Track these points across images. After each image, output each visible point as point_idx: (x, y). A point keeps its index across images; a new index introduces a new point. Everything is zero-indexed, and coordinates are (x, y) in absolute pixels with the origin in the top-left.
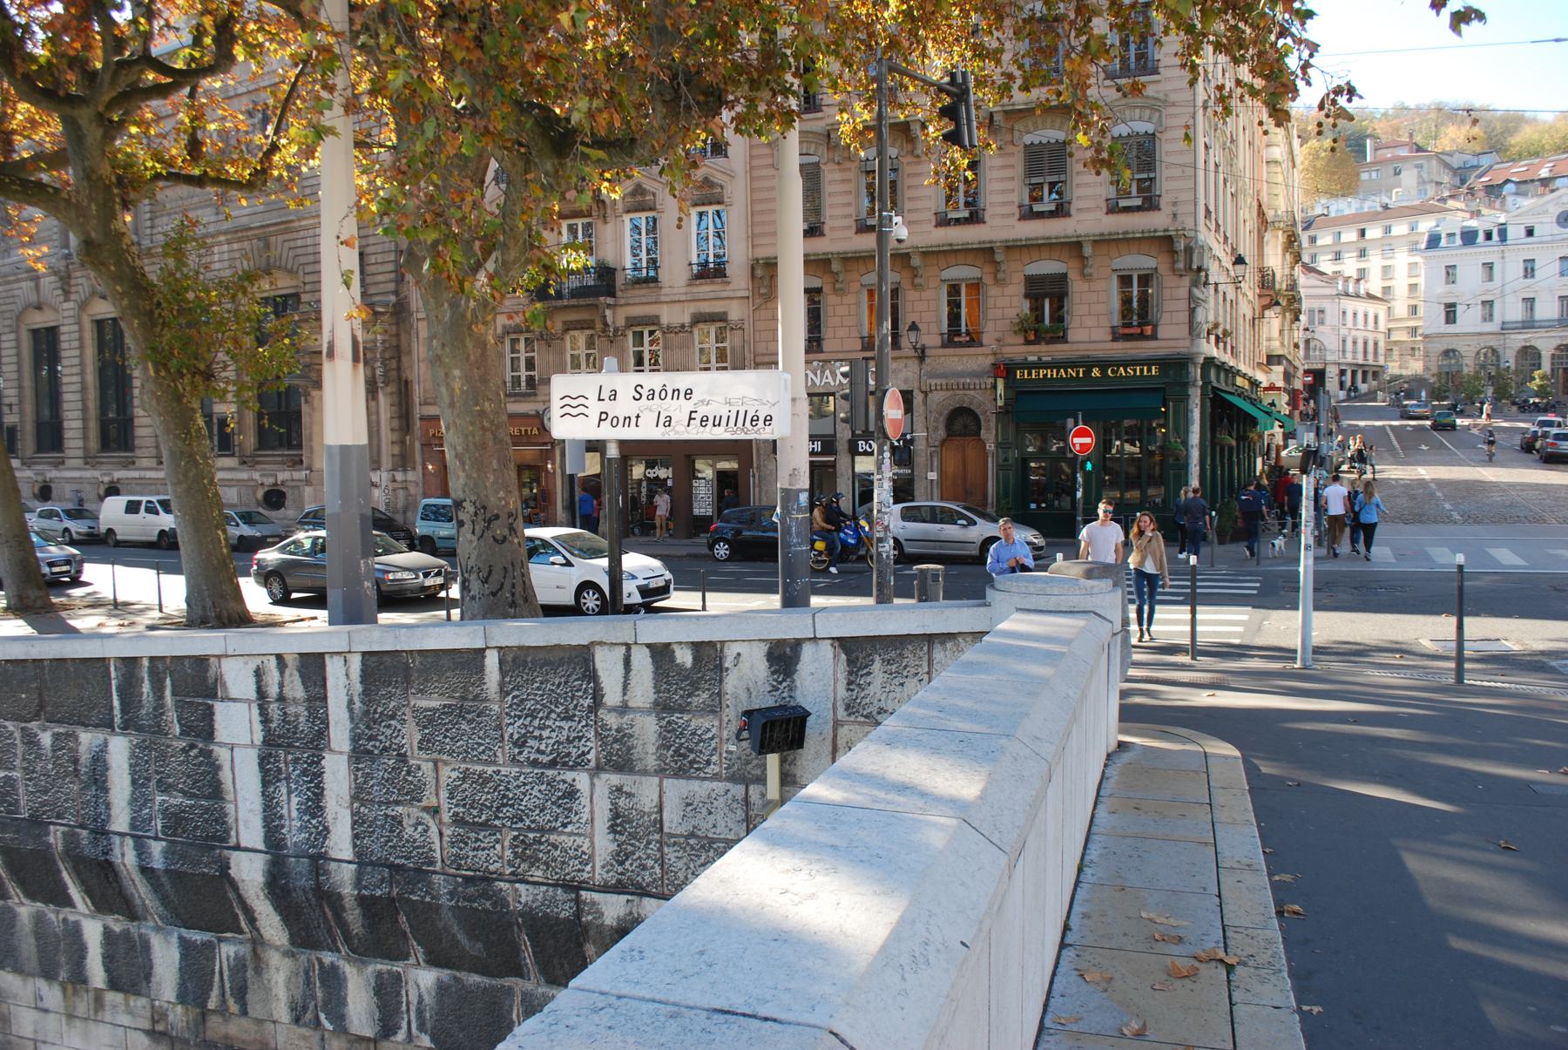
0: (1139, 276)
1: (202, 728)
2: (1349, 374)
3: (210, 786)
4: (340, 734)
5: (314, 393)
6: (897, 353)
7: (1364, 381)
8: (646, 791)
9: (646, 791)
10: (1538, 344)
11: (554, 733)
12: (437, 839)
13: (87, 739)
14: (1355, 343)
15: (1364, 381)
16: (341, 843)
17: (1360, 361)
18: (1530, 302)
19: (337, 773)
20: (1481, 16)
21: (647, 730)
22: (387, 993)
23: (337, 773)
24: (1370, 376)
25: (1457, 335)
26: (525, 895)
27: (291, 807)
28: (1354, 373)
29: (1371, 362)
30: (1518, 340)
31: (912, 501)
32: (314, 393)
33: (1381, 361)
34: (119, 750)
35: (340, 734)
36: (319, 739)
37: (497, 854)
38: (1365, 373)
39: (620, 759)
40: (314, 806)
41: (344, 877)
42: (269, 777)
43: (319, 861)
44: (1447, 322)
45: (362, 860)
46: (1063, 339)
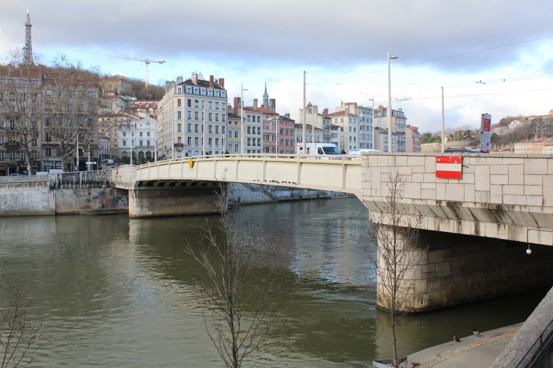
1: (79, 175)
2: (102, 157)
3: (79, 178)
4: (86, 175)
5: (432, 136)
6: (222, 151)
7: (105, 158)
8: (99, 176)
9: (99, 176)
10: (143, 151)
12: (90, 179)
13: (72, 176)
17: (104, 153)
19: (86, 177)
20: (165, 62)
21: (99, 174)
22: (86, 186)
23: (86, 177)
27: (83, 178)
28: (103, 157)
29: (107, 154)
30: (139, 150)
32: (432, 136)
33: (109, 154)
34: (74, 177)
35: (86, 175)
36: (85, 175)
37: (92, 179)
38: (105, 157)
39: (98, 175)
40: (84, 178)
43: (84, 180)
45: (87, 180)
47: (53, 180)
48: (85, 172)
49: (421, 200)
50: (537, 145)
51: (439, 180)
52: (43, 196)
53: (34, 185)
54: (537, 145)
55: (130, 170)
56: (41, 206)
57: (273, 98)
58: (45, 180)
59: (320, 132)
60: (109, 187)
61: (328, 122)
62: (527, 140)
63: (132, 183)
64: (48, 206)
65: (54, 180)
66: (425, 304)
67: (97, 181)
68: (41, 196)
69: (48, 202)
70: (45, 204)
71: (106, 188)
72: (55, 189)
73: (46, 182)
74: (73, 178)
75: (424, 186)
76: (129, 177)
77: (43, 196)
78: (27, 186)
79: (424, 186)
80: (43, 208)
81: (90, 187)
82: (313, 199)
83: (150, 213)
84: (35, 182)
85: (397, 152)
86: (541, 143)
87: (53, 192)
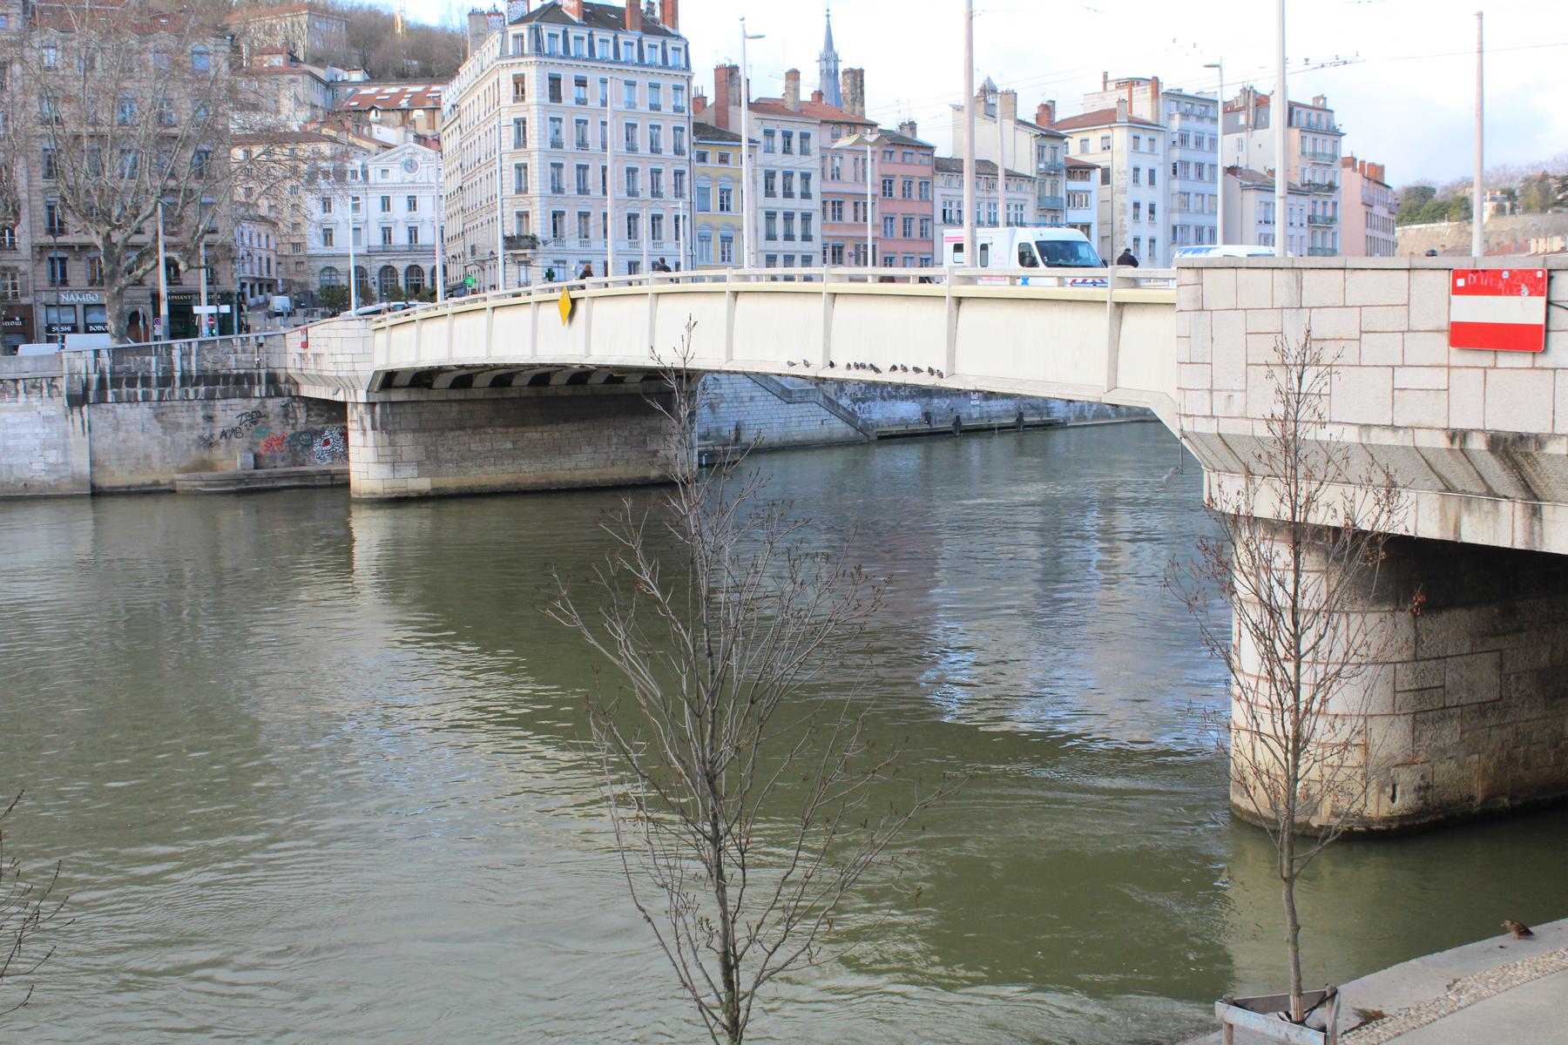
3: (171, 362)
4: (194, 352)
7: (261, 293)
11: (226, 350)
12: (209, 366)
13: (147, 358)
14: (260, 259)
16: (194, 368)
19: (193, 358)
21: (240, 349)
22: (196, 392)
23: (193, 358)
24: (265, 289)
25: (334, 256)
26: (222, 372)
27: (185, 364)
28: (252, 287)
29: (265, 275)
31: (349, 289)
34: (154, 359)
35: (194, 352)
36: (190, 353)
37: (218, 366)
39: (236, 352)
40: (189, 363)
42: (182, 360)
43: (190, 371)
44: (326, 244)
48: (190, 344)
49: (1393, 428)
51: (1459, 357)
52: (47, 430)
53: (13, 392)
55: (350, 333)
56: (38, 466)
58: (50, 374)
60: (279, 394)
61: (1055, 148)
64: (66, 464)
65: (84, 371)
67: (235, 372)
68: (39, 430)
69: (66, 452)
70: (53, 456)
71: (269, 396)
72: (88, 403)
73: (54, 378)
74: (149, 364)
75: (1404, 378)
76: (349, 358)
77: (47, 430)
79: (1404, 378)
80: (48, 472)
81: (210, 397)
82: (1003, 429)
83: (424, 484)
87: (81, 413)
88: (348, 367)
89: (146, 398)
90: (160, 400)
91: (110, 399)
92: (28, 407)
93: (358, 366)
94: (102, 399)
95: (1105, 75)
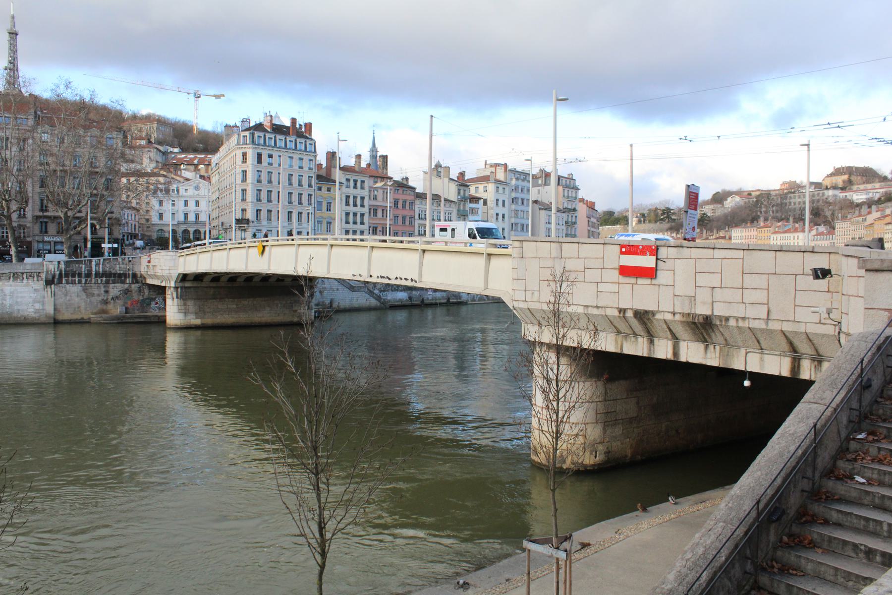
0: (169, 249)
3: (91, 267)
4: (101, 263)
10: (189, 229)
13: (81, 265)
15: (127, 240)
17: (130, 232)
18: (186, 216)
19: (101, 266)
21: (121, 262)
22: (101, 280)
23: (101, 266)
24: (133, 237)
25: (163, 225)
27: (97, 268)
28: (128, 236)
29: (133, 232)
34: (84, 266)
35: (101, 263)
36: (100, 264)
37: (112, 270)
38: (131, 236)
40: (99, 268)
41: (101, 272)
46: (96, 234)
47: (51, 271)
48: (99, 260)
49: (597, 307)
50: (763, 232)
51: (623, 279)
52: (36, 295)
53: (21, 278)
54: (763, 232)
55: (168, 257)
56: (31, 310)
57: (385, 154)
58: (38, 271)
59: (453, 205)
60: (137, 282)
62: (749, 225)
63: (171, 276)
64: (43, 309)
65: (53, 270)
66: (600, 458)
69: (43, 304)
70: (38, 306)
71: (133, 283)
73: (39, 273)
74: (82, 268)
75: (601, 287)
76: (168, 268)
78: (10, 278)
79: (601, 287)
80: (35, 313)
81: (107, 282)
83: (198, 322)
84: (23, 273)
85: (564, 238)
86: (769, 229)
87: (51, 288)
88: (167, 272)
89: (80, 282)
90: (86, 283)
91: (64, 282)
92: (28, 285)
93: (171, 272)
94: (60, 282)
95: (486, 162)
